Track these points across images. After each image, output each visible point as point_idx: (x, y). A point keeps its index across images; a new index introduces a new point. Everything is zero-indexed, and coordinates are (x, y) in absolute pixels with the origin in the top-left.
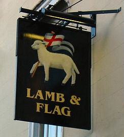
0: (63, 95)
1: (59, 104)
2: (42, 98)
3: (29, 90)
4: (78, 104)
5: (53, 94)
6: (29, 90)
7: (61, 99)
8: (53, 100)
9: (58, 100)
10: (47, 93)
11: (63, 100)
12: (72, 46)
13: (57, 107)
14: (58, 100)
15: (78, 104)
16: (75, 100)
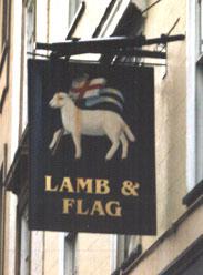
0: (106, 182)
1: (99, 197)
2: (71, 189)
3: (48, 179)
4: (135, 194)
5: (89, 181)
6: (48, 179)
7: (103, 189)
8: (90, 190)
9: (98, 191)
10: (81, 181)
11: (107, 190)
12: (115, 92)
13: (98, 203)
14: (98, 191)
15: (135, 194)
16: (129, 187)
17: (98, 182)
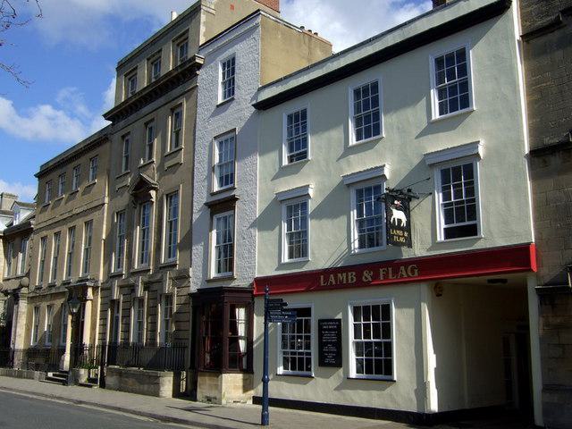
17: (350, 274)
